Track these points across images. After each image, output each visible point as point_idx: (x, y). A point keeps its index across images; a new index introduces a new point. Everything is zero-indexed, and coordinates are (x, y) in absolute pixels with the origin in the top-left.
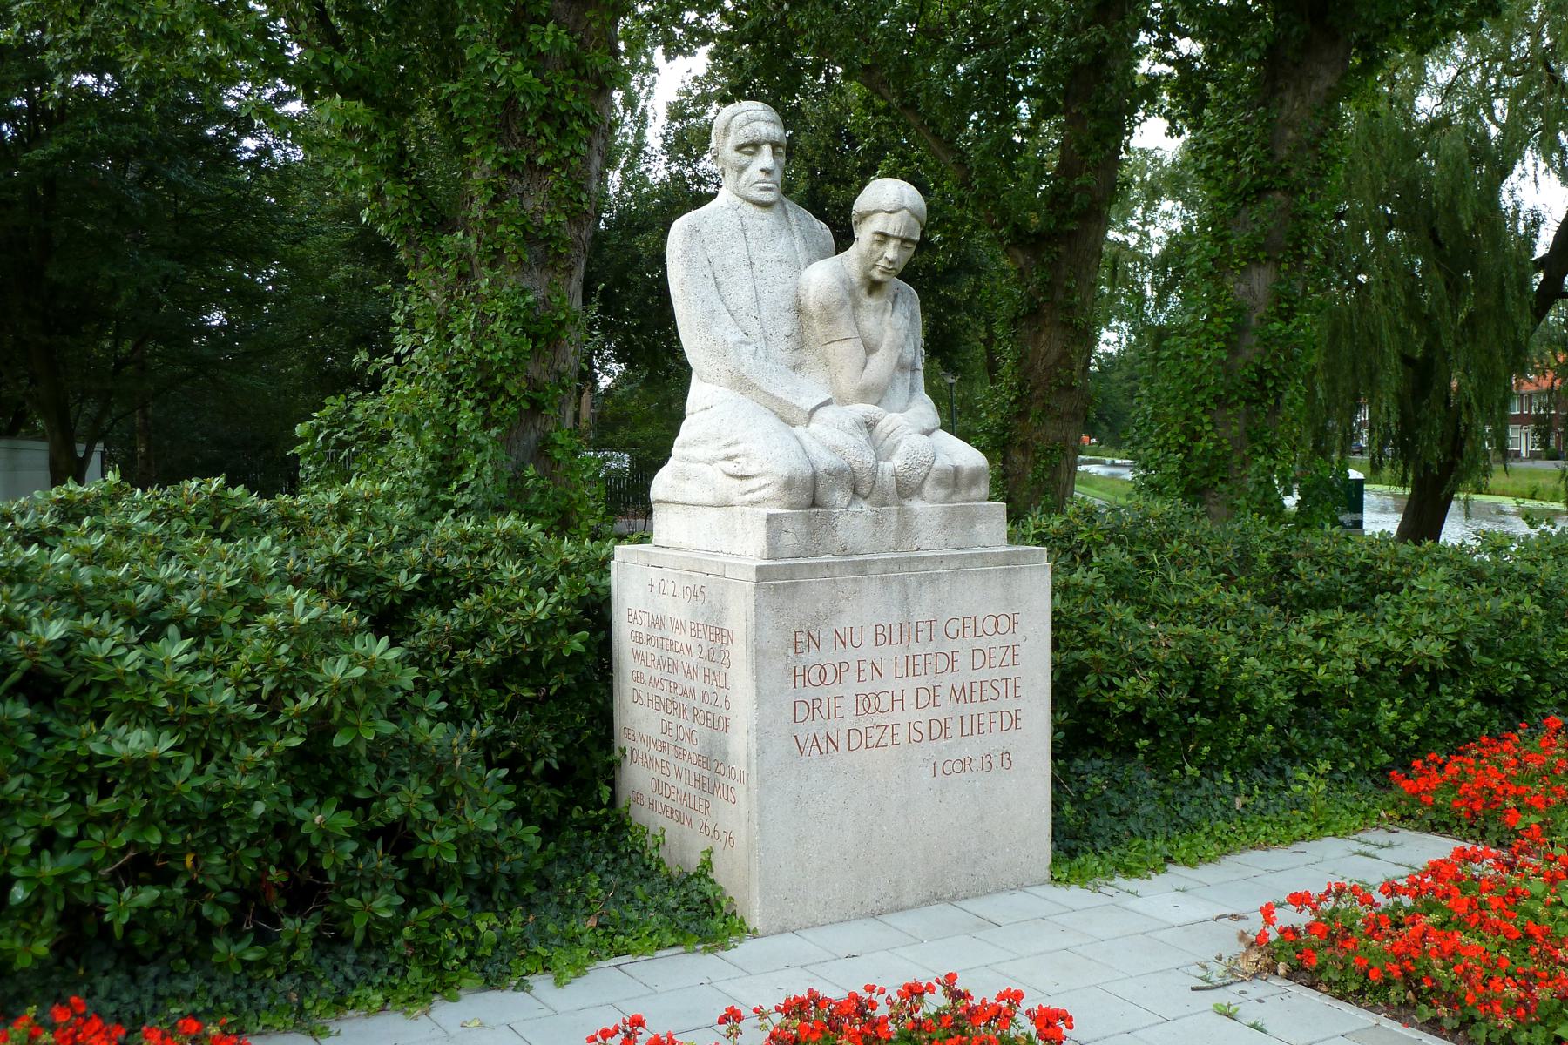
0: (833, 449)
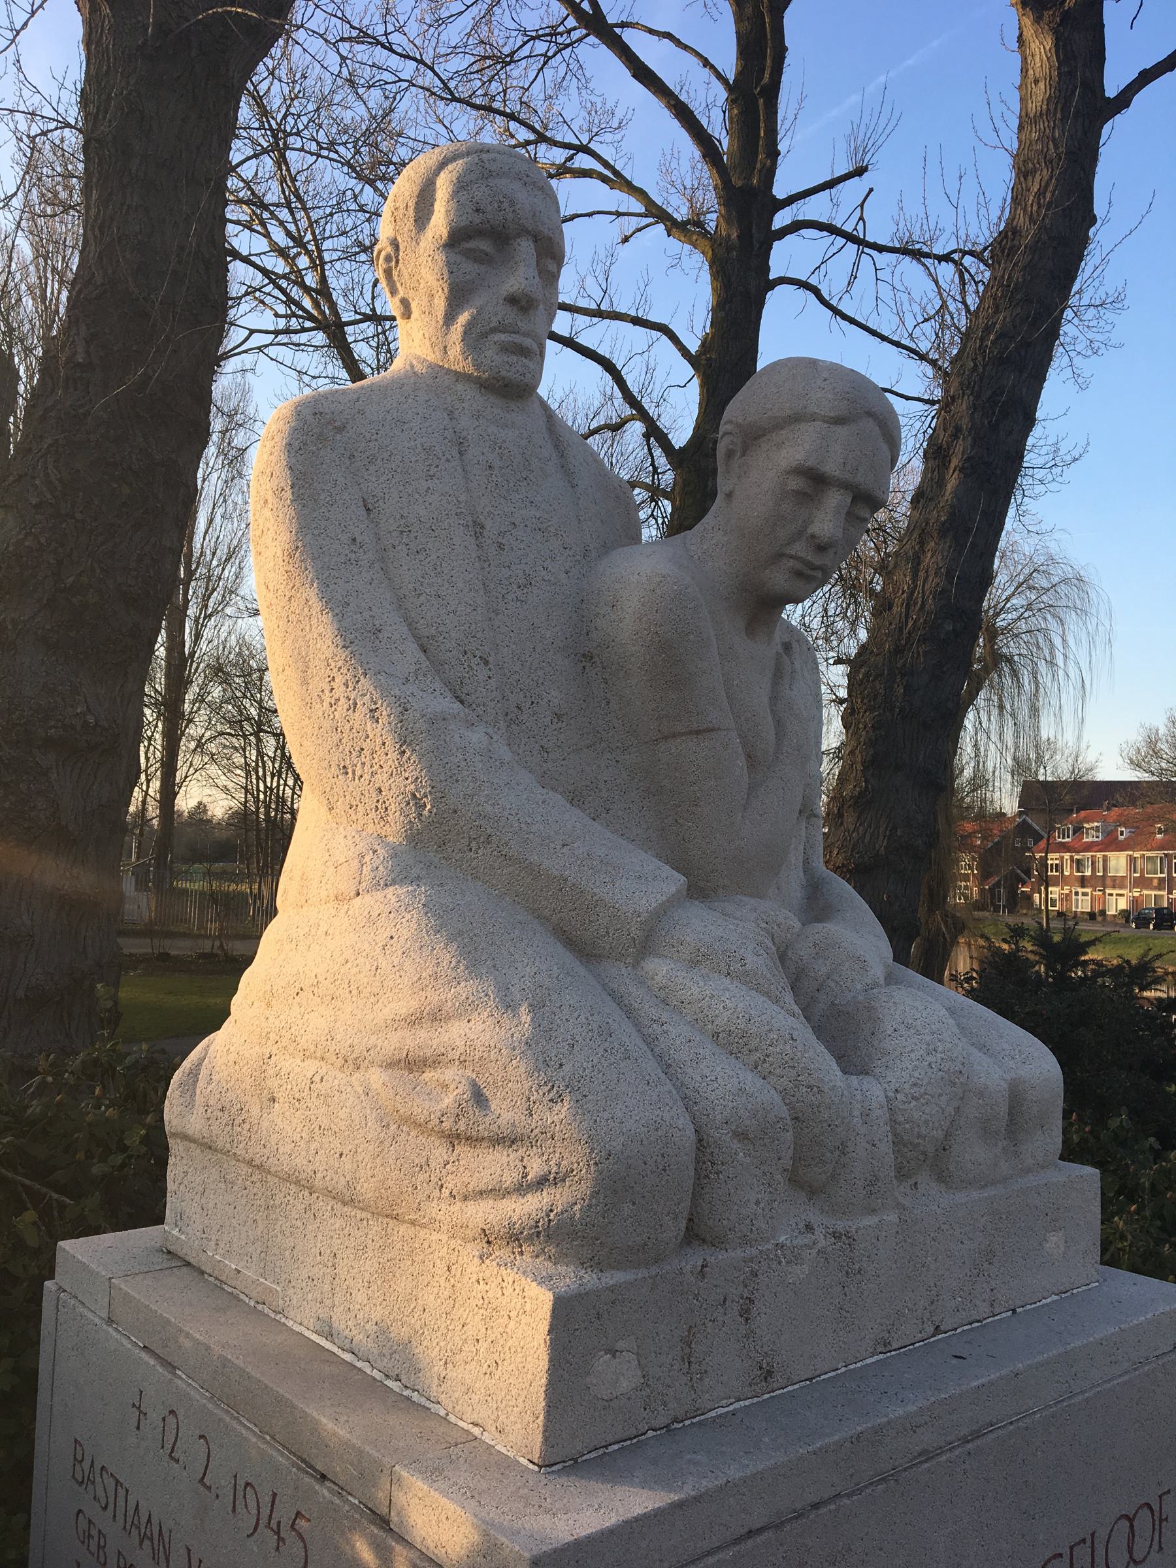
0: (733, 1043)
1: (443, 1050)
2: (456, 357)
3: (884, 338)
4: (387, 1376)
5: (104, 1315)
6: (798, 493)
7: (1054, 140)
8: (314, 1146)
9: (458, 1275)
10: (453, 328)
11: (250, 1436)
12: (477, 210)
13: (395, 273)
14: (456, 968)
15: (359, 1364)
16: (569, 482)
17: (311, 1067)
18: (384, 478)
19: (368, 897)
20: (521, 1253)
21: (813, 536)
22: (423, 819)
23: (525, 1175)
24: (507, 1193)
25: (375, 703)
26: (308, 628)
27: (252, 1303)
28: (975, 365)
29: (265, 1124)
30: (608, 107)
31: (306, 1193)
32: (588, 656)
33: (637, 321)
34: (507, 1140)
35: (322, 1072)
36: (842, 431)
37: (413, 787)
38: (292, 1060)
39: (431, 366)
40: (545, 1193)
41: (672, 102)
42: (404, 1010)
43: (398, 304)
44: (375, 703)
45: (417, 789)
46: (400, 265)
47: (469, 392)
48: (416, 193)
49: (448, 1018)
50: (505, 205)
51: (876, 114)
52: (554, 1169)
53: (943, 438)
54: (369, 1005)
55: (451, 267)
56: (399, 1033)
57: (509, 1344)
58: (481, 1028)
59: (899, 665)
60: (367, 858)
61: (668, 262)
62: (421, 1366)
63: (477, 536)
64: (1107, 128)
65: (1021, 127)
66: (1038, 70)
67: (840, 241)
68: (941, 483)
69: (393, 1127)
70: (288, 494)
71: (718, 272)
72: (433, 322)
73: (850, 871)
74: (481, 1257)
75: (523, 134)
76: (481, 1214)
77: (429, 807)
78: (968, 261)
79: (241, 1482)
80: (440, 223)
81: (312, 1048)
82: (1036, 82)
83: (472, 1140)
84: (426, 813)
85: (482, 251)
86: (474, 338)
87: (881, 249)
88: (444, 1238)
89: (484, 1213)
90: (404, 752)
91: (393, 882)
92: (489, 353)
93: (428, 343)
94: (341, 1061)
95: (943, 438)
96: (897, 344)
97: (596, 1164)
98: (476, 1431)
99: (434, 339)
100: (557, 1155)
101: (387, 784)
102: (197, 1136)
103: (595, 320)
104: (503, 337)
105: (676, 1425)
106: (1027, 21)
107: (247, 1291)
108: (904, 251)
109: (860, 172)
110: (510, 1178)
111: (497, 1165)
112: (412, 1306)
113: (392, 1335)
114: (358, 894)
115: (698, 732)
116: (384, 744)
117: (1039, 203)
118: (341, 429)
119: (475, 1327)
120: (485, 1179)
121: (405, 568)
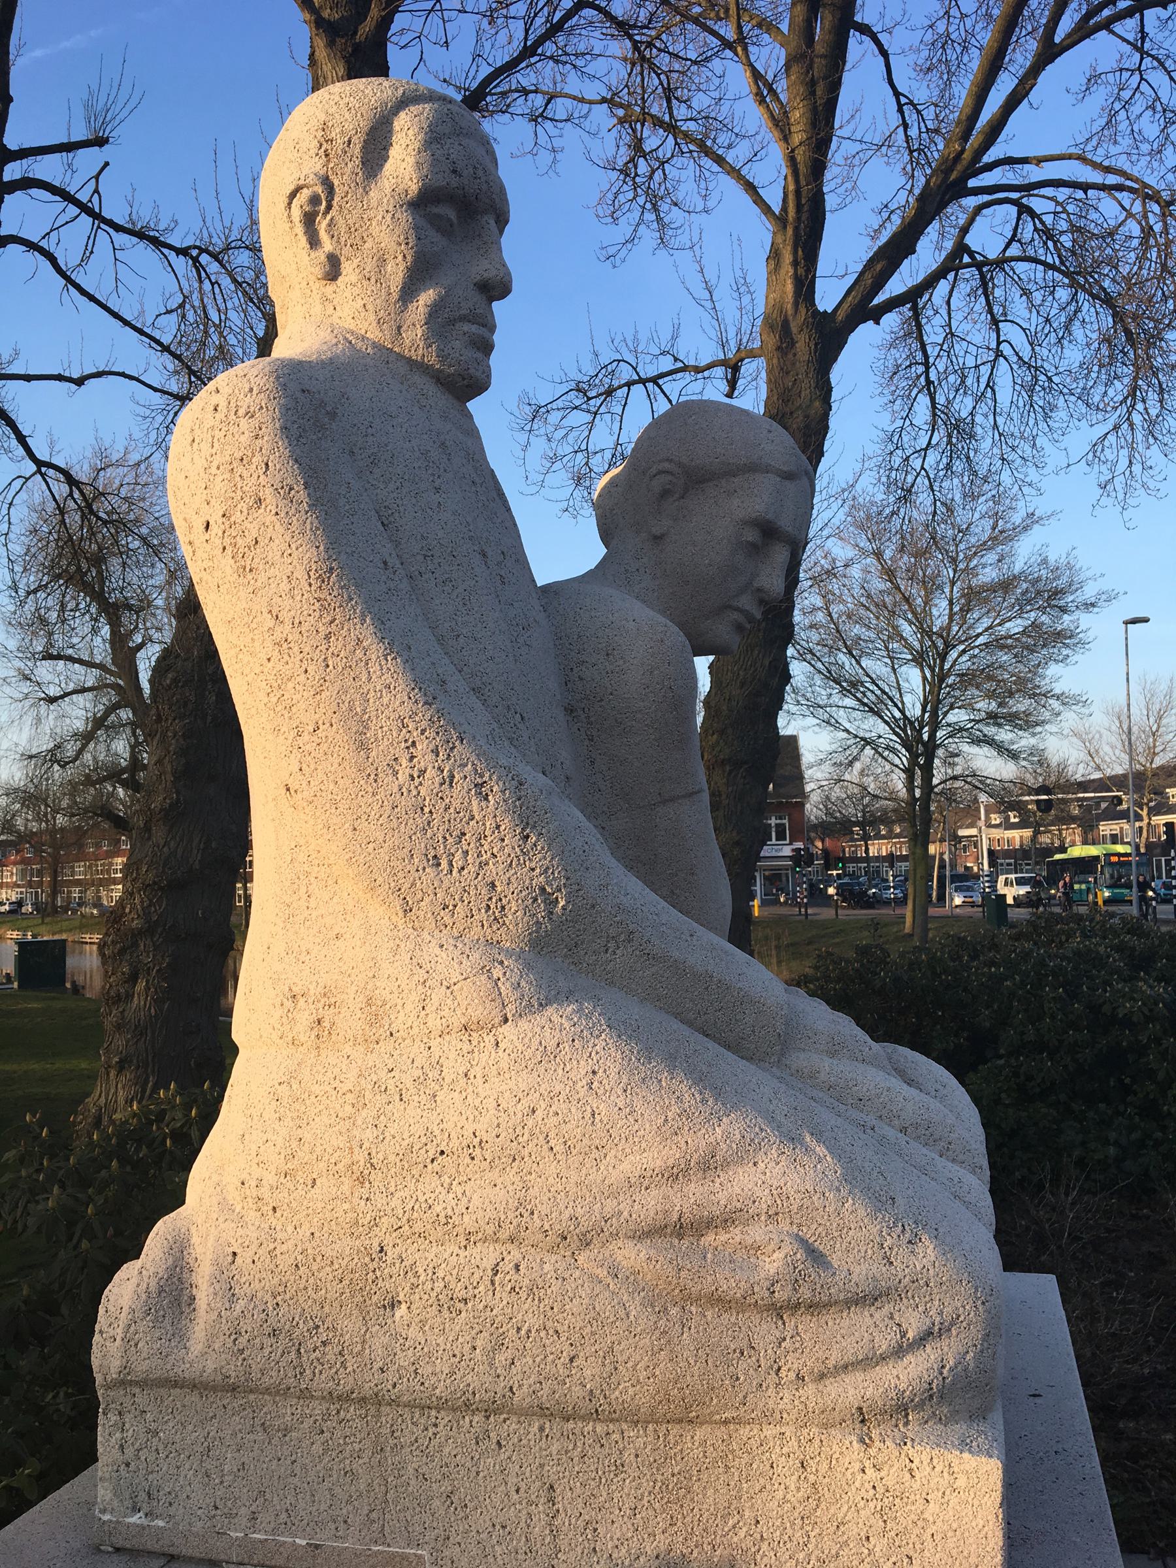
1: (739, 1205)
2: (414, 338)
3: (126, 323)
8: (502, 1358)
10: (412, 307)
12: (454, 172)
13: (322, 225)
14: (704, 1101)
17: (487, 1255)
18: (392, 486)
19: (523, 1024)
20: (906, 1424)
21: (759, 590)
22: (554, 917)
25: (481, 776)
29: (379, 1342)
34: (868, 1298)
35: (516, 1255)
42: (659, 1163)
43: (323, 258)
44: (481, 776)
45: (548, 883)
46: (333, 213)
47: (431, 388)
49: (726, 1164)
51: (115, 85)
52: (938, 1319)
56: (654, 1192)
58: (778, 1170)
59: (210, 671)
60: (497, 972)
67: (73, 210)
69: (674, 1311)
73: (161, 888)
74: (862, 1441)
76: (851, 1391)
77: (562, 903)
78: (204, 259)
81: (490, 1229)
83: (814, 1307)
84: (558, 909)
85: (449, 220)
86: (440, 321)
87: (118, 228)
88: (789, 1431)
89: (852, 1390)
90: (527, 837)
91: (549, 1002)
93: (372, 317)
94: (552, 1238)
96: (141, 332)
97: (983, 1303)
100: (936, 1303)
101: (505, 878)
104: (474, 328)
106: (320, 43)
108: (141, 235)
109: (100, 142)
110: (884, 1343)
112: (731, 1523)
114: (506, 1020)
116: (498, 827)
121: (437, 602)
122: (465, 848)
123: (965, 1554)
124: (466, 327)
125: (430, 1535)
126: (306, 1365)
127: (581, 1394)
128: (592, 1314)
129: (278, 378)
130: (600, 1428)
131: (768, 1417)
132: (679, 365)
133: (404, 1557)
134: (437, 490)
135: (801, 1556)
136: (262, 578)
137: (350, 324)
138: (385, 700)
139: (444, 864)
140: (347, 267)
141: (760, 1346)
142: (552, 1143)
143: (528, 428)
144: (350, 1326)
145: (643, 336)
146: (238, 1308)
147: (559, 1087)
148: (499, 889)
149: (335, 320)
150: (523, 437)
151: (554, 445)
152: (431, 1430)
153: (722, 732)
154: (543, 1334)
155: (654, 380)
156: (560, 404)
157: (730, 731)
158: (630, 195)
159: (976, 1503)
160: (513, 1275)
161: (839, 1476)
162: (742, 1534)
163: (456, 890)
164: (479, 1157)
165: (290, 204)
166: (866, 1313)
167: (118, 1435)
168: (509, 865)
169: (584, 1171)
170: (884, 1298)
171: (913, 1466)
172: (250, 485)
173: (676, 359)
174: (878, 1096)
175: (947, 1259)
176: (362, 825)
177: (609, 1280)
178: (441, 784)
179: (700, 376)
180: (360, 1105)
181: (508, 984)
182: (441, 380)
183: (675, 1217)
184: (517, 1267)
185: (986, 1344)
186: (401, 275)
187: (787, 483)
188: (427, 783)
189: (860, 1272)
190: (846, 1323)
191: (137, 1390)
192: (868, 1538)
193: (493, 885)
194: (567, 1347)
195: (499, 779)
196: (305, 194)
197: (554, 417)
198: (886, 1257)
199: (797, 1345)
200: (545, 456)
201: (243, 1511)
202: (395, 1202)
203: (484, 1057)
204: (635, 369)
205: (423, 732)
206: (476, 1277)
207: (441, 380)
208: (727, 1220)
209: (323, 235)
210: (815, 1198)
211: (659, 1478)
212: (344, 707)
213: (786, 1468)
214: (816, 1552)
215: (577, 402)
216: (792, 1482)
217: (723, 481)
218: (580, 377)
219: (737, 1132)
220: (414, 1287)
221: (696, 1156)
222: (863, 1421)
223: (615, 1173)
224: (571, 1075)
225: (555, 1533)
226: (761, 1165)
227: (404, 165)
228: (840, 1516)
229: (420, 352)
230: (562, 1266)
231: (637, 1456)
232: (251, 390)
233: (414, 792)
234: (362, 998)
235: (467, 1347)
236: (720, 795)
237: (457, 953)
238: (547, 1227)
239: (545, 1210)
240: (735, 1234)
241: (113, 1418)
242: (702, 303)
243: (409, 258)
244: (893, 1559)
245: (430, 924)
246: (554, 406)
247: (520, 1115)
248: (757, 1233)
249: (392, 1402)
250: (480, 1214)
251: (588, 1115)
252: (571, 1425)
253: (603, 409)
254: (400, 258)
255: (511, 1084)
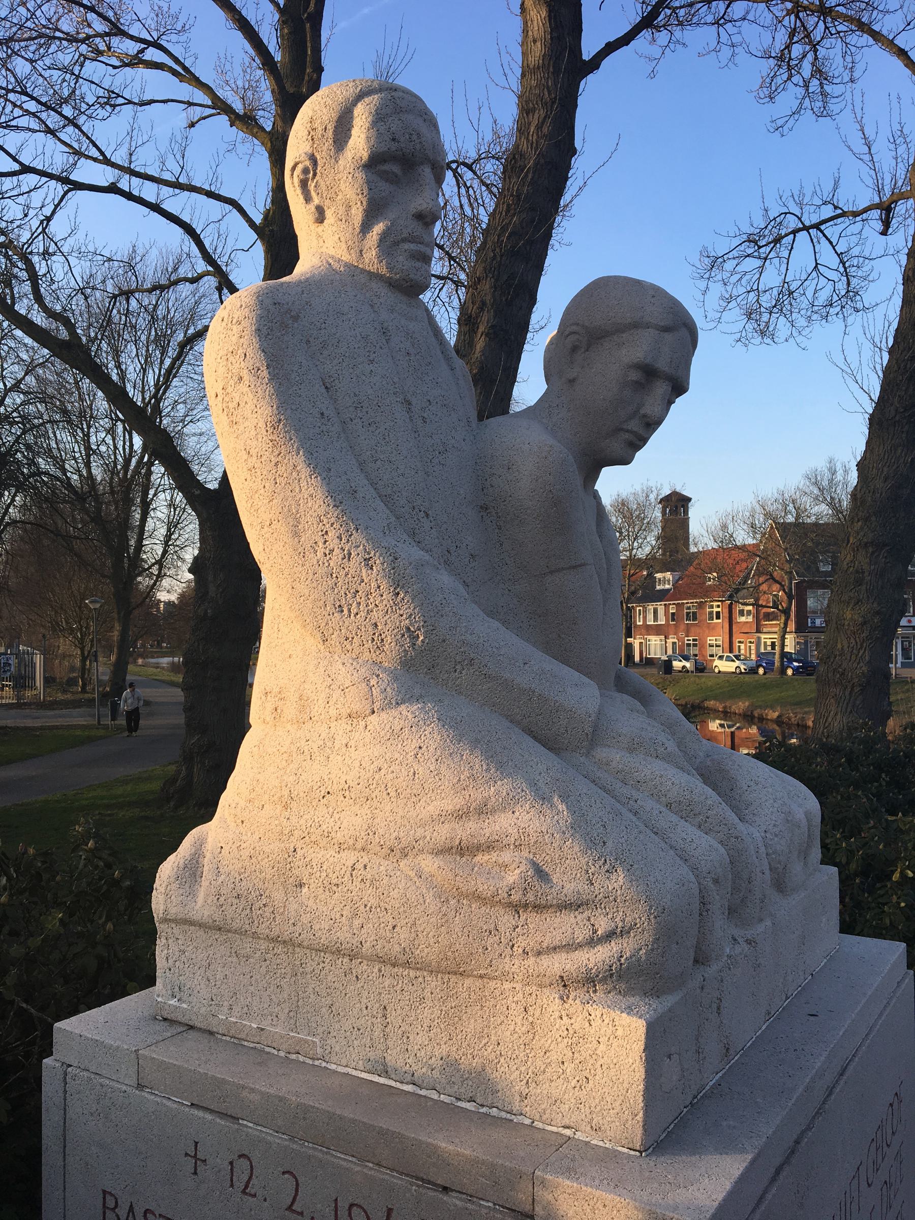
1: (497, 837)
2: (371, 259)
4: (459, 1099)
5: (133, 1082)
6: (636, 382)
7: (548, 87)
8: (357, 923)
9: (536, 1015)
10: (368, 236)
11: (352, 1166)
12: (394, 140)
13: (311, 186)
14: (488, 770)
15: (423, 1092)
16: (449, 365)
17: (349, 857)
18: (336, 362)
19: (384, 715)
20: (595, 991)
21: (644, 416)
22: (416, 647)
23: (595, 932)
24: (580, 946)
25: (369, 554)
26: (297, 490)
27: (282, 1054)
28: (495, 255)
29: (293, 907)
30: (172, 12)
31: (346, 960)
32: (490, 508)
33: (210, 195)
35: (365, 860)
36: (668, 337)
37: (407, 621)
38: (322, 852)
39: (348, 265)
40: (613, 943)
41: (237, 17)
42: (450, 807)
43: (313, 209)
44: (369, 554)
47: (384, 291)
48: (335, 118)
49: (493, 811)
50: (414, 137)
52: (620, 925)
53: (473, 310)
54: (410, 804)
55: (370, 184)
56: (446, 826)
57: (599, 1063)
58: (528, 817)
60: (373, 682)
61: (225, 147)
62: (499, 1087)
63: (409, 411)
64: (582, 83)
65: (523, 75)
66: (535, 33)
68: (471, 344)
69: (453, 902)
70: (265, 373)
71: (276, 160)
72: (350, 229)
74: (561, 998)
75: (100, 26)
76: (557, 965)
77: (421, 638)
78: (462, 170)
79: (343, 1205)
80: (359, 142)
81: (351, 842)
82: (535, 41)
83: (538, 908)
84: (419, 642)
86: (387, 245)
88: (518, 986)
89: (558, 964)
90: (398, 594)
92: (401, 259)
93: (344, 246)
94: (386, 851)
95: (473, 310)
97: (655, 917)
98: (568, 1132)
99: (350, 243)
101: (383, 621)
102: (205, 919)
103: (177, 191)
104: (412, 246)
105: (696, 1100)
107: (274, 1045)
110: (581, 935)
111: (569, 925)
112: (484, 1042)
113: (462, 1066)
114: (373, 712)
115: (574, 567)
116: (379, 587)
117: (537, 135)
118: (296, 318)
119: (559, 1051)
120: (557, 937)
121: (363, 438)
122: (359, 600)
123: (621, 1080)
124: (406, 246)
125: (320, 1030)
126: (255, 917)
127: (399, 950)
128: (405, 899)
129: (257, 297)
130: (412, 973)
131: (505, 976)
132: (839, 211)
133: (306, 1041)
134: (372, 362)
135: (523, 1069)
136: (241, 428)
137: (332, 252)
138: (310, 505)
139: (346, 611)
140: (329, 213)
141: (502, 930)
142: (389, 791)
143: (707, 276)
144: (278, 896)
145: (808, 192)
146: (221, 879)
147: (397, 755)
148: (380, 628)
149: (324, 250)
150: (702, 284)
151: (729, 288)
152: (322, 965)
153: (866, 519)
154: (378, 910)
155: (817, 226)
156: (735, 253)
157: (873, 518)
158: (785, 76)
159: (629, 1048)
160: (362, 872)
161: (547, 1019)
162: (489, 1050)
163: (353, 628)
164: (348, 797)
165: (292, 175)
166: (572, 915)
167: (166, 952)
168: (387, 613)
169: (406, 810)
170: (585, 907)
171: (591, 1018)
172: (235, 369)
173: (836, 207)
174: (652, 780)
175: (632, 885)
176: (297, 585)
177: (416, 879)
178: (343, 559)
179: (858, 219)
180: (289, 762)
181: (378, 690)
182: (393, 284)
183: (457, 843)
184: (365, 867)
185: (655, 945)
186: (360, 215)
187: (666, 335)
188: (334, 558)
189: (570, 888)
190: (558, 920)
191: (174, 925)
192: (563, 1063)
193: (376, 625)
194: (391, 920)
195: (381, 555)
196: (300, 167)
197: (729, 265)
198: (589, 879)
199: (525, 931)
200: (722, 298)
201: (226, 1003)
202: (302, 821)
203: (357, 734)
204: (800, 219)
205: (332, 525)
206: (343, 871)
207: (393, 284)
208: (489, 847)
209: (313, 194)
210: (546, 837)
211: (444, 1008)
212: (286, 510)
213: (516, 1011)
214: (532, 1068)
215: (750, 251)
216: (519, 1020)
217: (615, 337)
218: (751, 230)
219: (504, 791)
220: (311, 874)
221: (474, 804)
222: (565, 986)
223: (424, 812)
224: (405, 749)
225: (386, 1037)
226: (517, 814)
227: (359, 140)
228: (547, 1045)
229: (375, 267)
230: (391, 868)
231: (432, 993)
232: (241, 306)
233: (327, 564)
234: (297, 695)
235: (338, 916)
236: (863, 573)
237: (352, 668)
238: (382, 843)
239: (381, 831)
240: (494, 856)
241: (164, 941)
242: (862, 157)
243: (364, 203)
244: (577, 1078)
245: (338, 649)
246: (730, 255)
247: (371, 772)
248: (506, 856)
249: (300, 945)
250: (346, 832)
251: (411, 773)
252: (396, 970)
253: (772, 255)
254: (359, 203)
255: (370, 752)
